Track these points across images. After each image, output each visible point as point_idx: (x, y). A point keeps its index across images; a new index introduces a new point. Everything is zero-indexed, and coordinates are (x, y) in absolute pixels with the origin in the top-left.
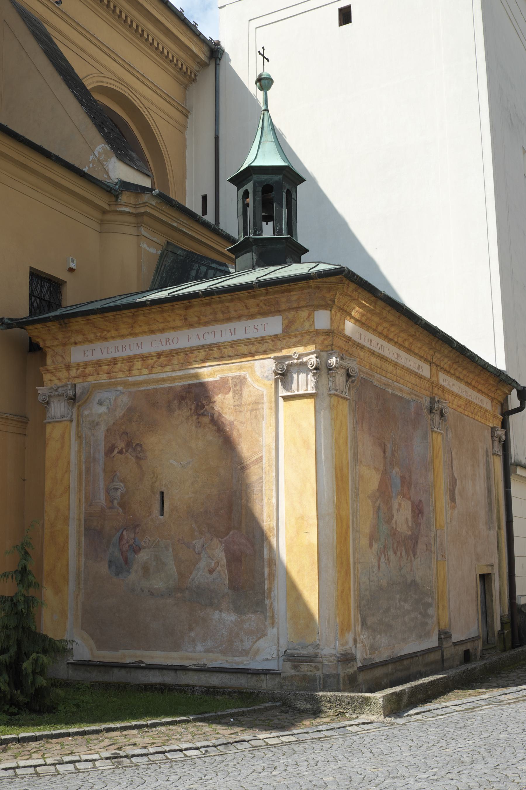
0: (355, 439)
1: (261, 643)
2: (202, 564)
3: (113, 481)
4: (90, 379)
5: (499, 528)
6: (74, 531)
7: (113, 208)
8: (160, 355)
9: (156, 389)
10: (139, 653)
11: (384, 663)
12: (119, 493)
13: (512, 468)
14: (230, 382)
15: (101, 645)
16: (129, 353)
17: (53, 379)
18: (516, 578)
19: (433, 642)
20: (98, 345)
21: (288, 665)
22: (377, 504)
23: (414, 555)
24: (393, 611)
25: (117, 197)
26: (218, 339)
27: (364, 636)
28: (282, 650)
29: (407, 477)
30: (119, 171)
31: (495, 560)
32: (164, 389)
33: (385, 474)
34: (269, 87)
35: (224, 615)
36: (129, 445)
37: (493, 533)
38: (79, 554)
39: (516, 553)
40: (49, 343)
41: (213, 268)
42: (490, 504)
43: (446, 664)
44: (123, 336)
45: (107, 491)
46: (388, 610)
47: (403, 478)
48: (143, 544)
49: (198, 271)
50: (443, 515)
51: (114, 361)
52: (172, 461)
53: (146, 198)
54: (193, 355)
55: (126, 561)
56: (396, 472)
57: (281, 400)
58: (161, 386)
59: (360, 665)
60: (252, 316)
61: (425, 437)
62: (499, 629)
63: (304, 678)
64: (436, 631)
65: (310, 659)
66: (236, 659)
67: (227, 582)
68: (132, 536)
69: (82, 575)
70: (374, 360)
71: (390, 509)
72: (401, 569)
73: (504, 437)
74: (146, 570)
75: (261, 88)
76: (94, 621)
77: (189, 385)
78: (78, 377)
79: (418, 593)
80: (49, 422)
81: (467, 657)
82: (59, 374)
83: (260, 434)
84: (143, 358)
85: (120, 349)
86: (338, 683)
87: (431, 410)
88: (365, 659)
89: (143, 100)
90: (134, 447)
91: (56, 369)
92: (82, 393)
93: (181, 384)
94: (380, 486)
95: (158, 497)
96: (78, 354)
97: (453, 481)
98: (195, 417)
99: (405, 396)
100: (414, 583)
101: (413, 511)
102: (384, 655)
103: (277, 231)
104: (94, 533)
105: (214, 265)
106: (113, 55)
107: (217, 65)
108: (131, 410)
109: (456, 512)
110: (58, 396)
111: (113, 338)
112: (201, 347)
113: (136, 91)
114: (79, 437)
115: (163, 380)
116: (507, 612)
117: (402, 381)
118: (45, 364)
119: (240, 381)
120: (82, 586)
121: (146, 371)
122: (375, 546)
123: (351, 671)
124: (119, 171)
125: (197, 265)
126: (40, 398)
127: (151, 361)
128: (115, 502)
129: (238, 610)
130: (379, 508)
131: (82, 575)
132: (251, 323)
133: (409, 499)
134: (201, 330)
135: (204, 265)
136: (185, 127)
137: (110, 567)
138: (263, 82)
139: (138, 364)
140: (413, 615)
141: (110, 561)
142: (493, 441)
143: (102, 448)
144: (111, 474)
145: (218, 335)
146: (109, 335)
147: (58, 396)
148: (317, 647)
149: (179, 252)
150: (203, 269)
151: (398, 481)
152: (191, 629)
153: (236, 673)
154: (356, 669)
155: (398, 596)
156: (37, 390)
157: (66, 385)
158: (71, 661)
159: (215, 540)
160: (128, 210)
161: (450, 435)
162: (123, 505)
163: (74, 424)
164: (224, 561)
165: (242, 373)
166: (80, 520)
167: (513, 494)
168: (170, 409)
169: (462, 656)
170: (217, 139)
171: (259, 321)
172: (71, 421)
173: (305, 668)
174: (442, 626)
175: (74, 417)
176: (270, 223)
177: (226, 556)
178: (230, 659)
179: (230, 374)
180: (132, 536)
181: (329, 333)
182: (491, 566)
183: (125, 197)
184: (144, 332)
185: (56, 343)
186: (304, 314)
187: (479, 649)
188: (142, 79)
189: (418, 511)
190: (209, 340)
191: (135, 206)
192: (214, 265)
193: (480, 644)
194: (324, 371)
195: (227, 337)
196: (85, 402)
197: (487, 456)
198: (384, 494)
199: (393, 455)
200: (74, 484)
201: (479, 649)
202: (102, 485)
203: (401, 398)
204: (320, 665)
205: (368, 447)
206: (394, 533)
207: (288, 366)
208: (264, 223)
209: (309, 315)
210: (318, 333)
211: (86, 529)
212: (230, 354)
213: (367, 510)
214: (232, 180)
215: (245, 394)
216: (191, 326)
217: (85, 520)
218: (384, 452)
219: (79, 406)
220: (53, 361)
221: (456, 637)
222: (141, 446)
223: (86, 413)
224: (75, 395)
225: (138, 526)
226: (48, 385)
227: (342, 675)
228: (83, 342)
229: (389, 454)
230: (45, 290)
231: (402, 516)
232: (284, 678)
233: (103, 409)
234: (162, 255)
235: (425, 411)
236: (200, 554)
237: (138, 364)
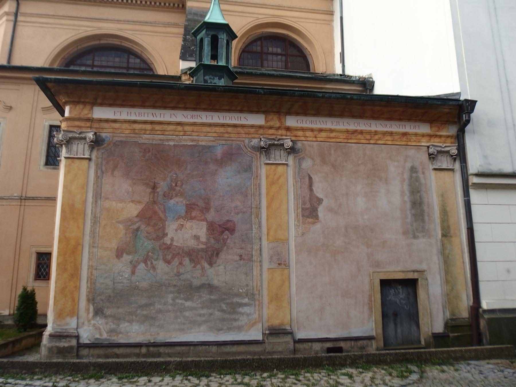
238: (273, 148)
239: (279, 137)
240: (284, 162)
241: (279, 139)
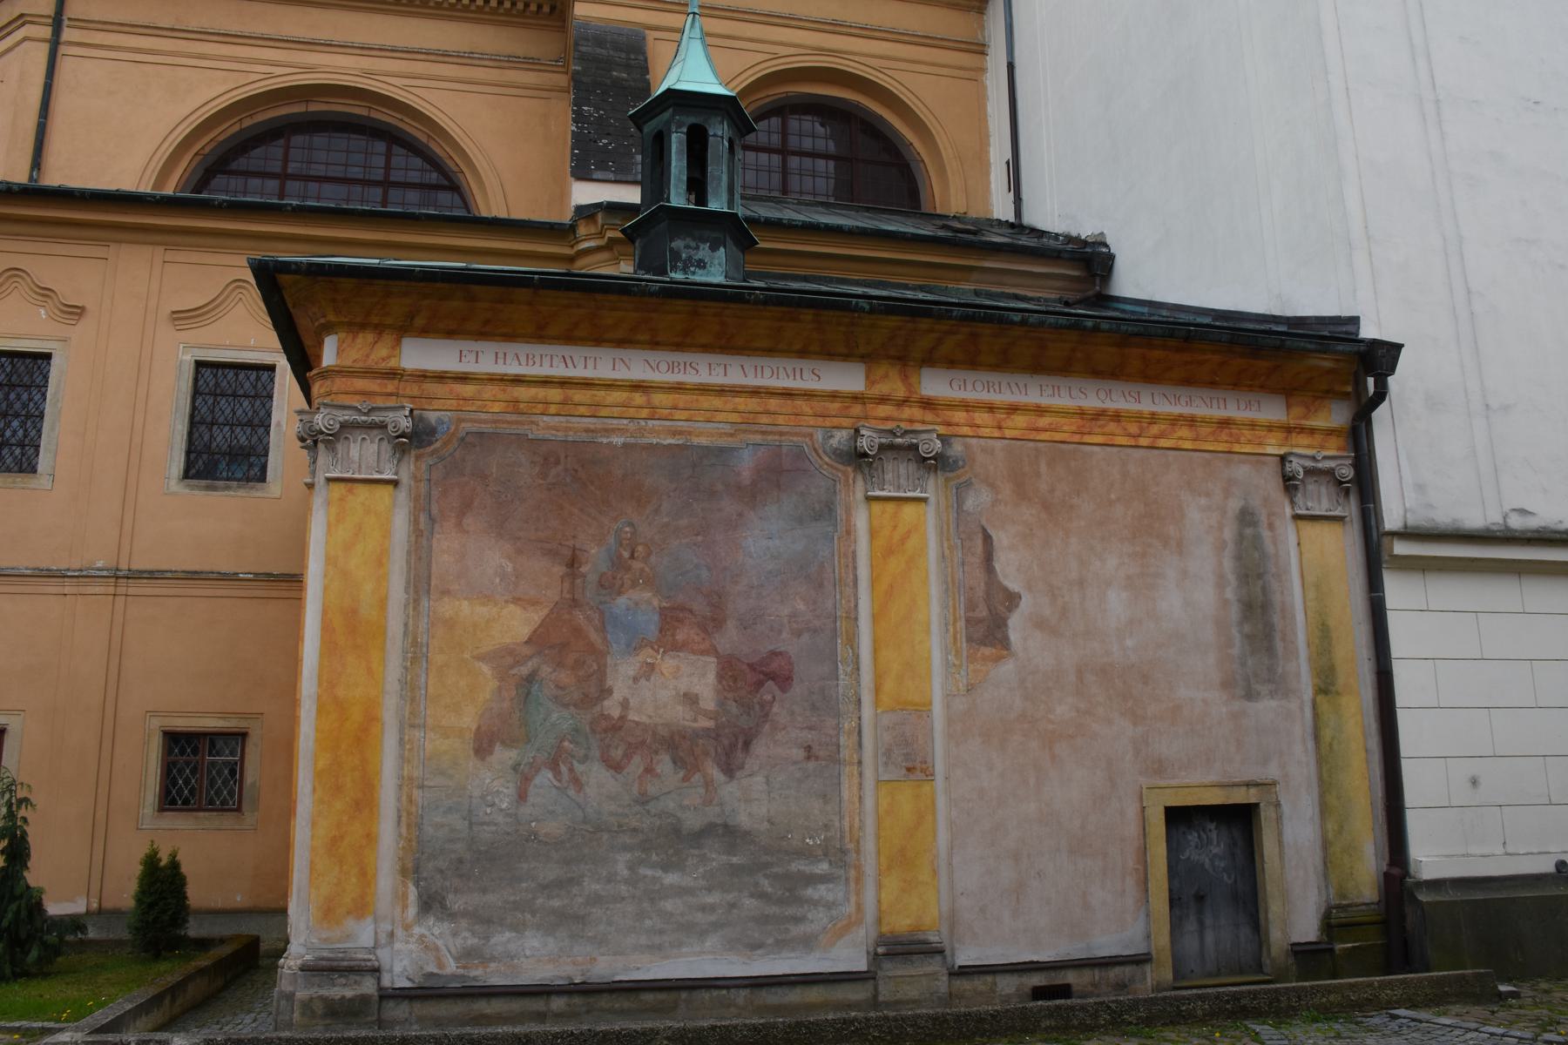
5: (1326, 686)
70: (741, 402)
89: (862, 59)
160: (592, 244)
183: (582, 230)
191: (601, 234)
238: (890, 454)
239: (904, 426)
240: (917, 494)
241: (906, 432)
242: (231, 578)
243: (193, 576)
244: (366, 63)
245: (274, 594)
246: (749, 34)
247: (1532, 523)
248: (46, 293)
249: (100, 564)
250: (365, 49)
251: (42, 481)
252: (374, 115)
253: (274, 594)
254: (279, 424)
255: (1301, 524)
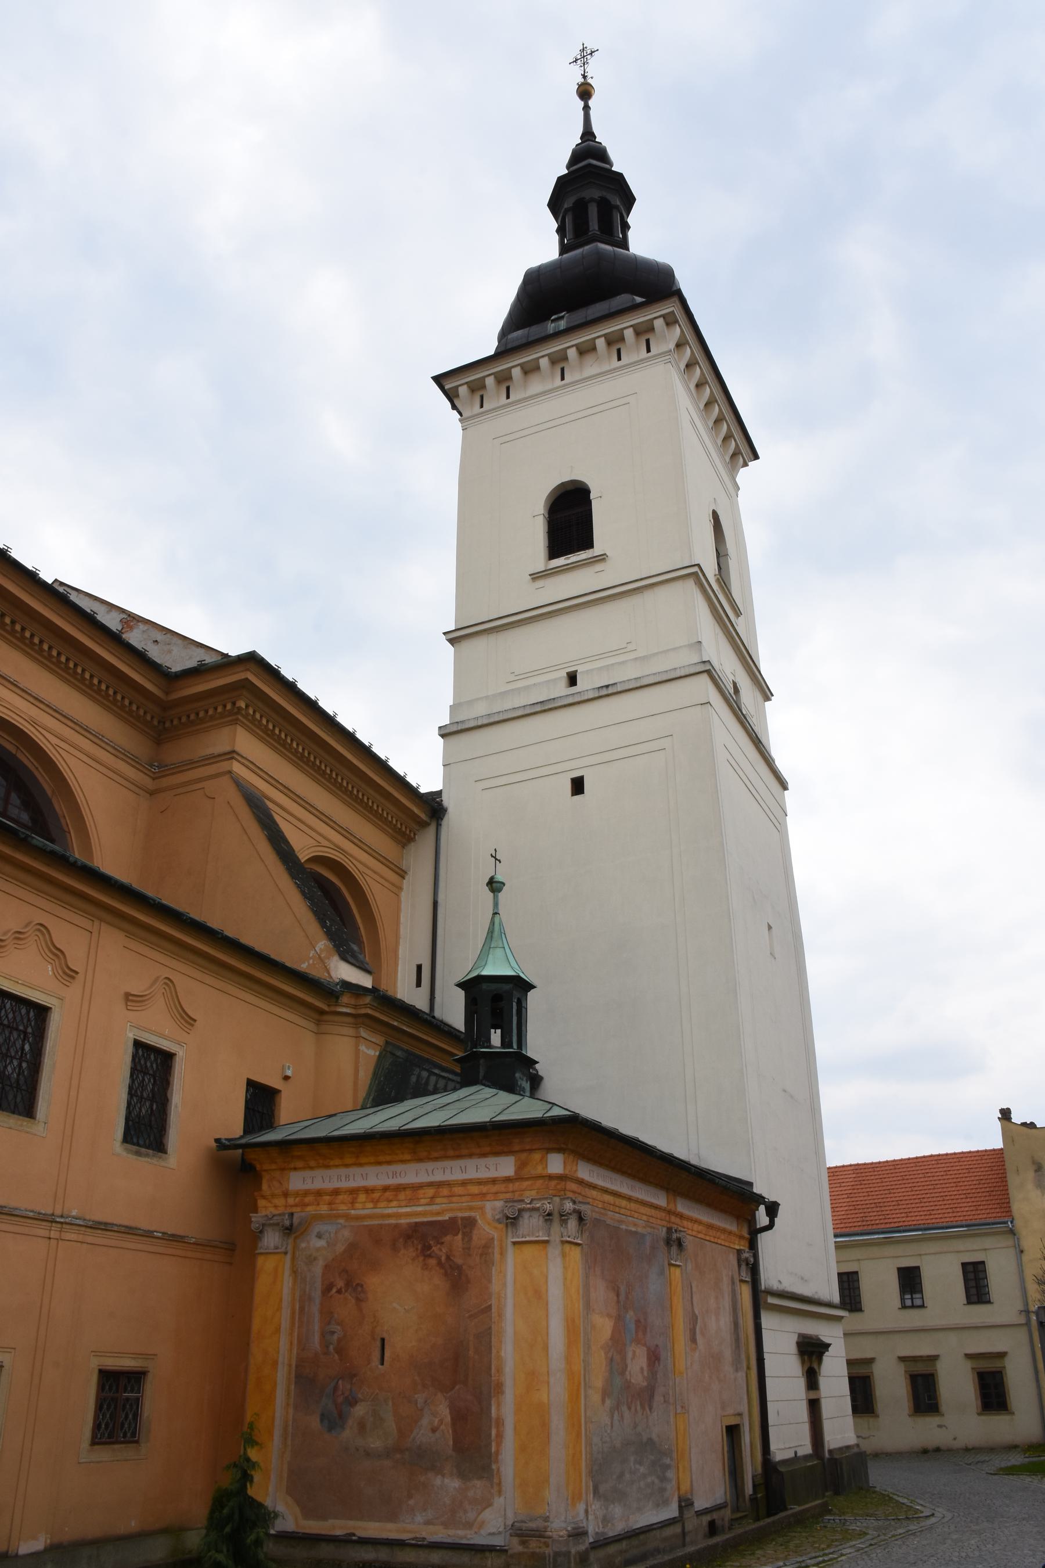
0: (587, 1287)
1: (487, 1514)
2: (425, 1422)
3: (329, 1323)
4: (309, 1208)
5: (748, 1368)
6: (282, 1376)
7: (333, 1009)
8: (386, 1189)
9: (381, 1225)
10: (351, 1523)
11: (618, 1539)
12: (335, 1337)
13: (762, 1295)
14: (460, 1222)
15: (308, 1513)
16: (352, 1184)
17: (267, 1208)
18: (770, 1429)
19: (671, 1511)
20: (319, 1173)
21: (515, 1540)
22: (610, 1355)
23: (650, 1409)
24: (627, 1476)
25: (337, 998)
26: (448, 1177)
27: (596, 1506)
28: (510, 1523)
29: (642, 1320)
30: (345, 972)
31: (744, 1408)
32: (389, 1225)
33: (619, 1319)
34: (500, 890)
35: (446, 1481)
36: (348, 1284)
37: (741, 1375)
38: (288, 1405)
39: (769, 1397)
40: (266, 1167)
41: (436, 1074)
42: (737, 1340)
43: (688, 1539)
44: (347, 1166)
45: (323, 1335)
46: (621, 1475)
47: (638, 1322)
48: (360, 1396)
49: (419, 1076)
50: (684, 1359)
51: (336, 1192)
52: (395, 1305)
53: (368, 999)
54: (421, 1192)
55: (341, 1415)
56: (630, 1316)
57: (510, 1245)
58: (387, 1222)
59: (591, 1540)
60: (484, 1155)
61: (662, 1273)
62: (751, 1492)
63: (533, 1554)
64: (676, 1499)
65: (539, 1534)
66: (460, 1533)
67: (451, 1443)
68: (348, 1387)
69: (290, 1429)
70: (608, 1198)
71: (624, 1358)
72: (635, 1426)
73: (752, 1260)
74: (362, 1426)
75: (493, 890)
76: (299, 1486)
77: (416, 1223)
78: (296, 1206)
79: (656, 1455)
80: (261, 1254)
81: (713, 1529)
82: (276, 1201)
83: (490, 1281)
84: (368, 1190)
85: (343, 1178)
86: (569, 1562)
87: (668, 1242)
88: (597, 1533)
90: (354, 1287)
91: (273, 1196)
92: (300, 1224)
93: (408, 1221)
94: (613, 1332)
95: (379, 1343)
96: (299, 1181)
97: (694, 1319)
98: (421, 1258)
99: (640, 1230)
100: (650, 1441)
101: (649, 1359)
102: (619, 1527)
103: (505, 1042)
104: (306, 1380)
105: (436, 1071)
106: (331, 823)
107: (439, 826)
108: (352, 1247)
109: (697, 1354)
110: (271, 1225)
111: (337, 1166)
112: (431, 1184)
113: (351, 856)
114: (294, 1272)
115: (389, 1216)
116: (759, 1470)
117: (636, 1215)
118: (260, 1189)
119: (470, 1223)
120: (289, 1442)
121: (371, 1205)
122: (608, 1402)
123: (582, 1548)
124: (345, 972)
125: (418, 1070)
126: (254, 1226)
127: (376, 1195)
128: (331, 1347)
129: (462, 1475)
130: (612, 1360)
131: (290, 1429)
132: (482, 1162)
133: (645, 1345)
134: (430, 1165)
135: (425, 1069)
136: (401, 889)
137: (322, 1421)
138: (494, 885)
139: (362, 1197)
140: (649, 1480)
141: (322, 1415)
142: (739, 1266)
143: (319, 1285)
144: (327, 1315)
145: (448, 1171)
146: (332, 1163)
147: (271, 1225)
148: (546, 1519)
149: (399, 1053)
150: (425, 1074)
151: (633, 1326)
152: (410, 1497)
153: (459, 1549)
154: (587, 1545)
155: (632, 1458)
156: (250, 1218)
157: (283, 1214)
158: (272, 1532)
159: (439, 1395)
161: (690, 1267)
162: (339, 1351)
163: (289, 1257)
164: (448, 1419)
165: (473, 1214)
166: (290, 1365)
167: (763, 1326)
168: (395, 1249)
169: (707, 1529)
170: (435, 904)
171: (491, 1161)
172: (286, 1253)
173: (534, 1545)
174: (682, 1492)
175: (290, 1248)
176: (499, 1031)
177: (451, 1413)
178: (451, 1532)
179: (460, 1215)
180: (348, 1387)
181: (561, 1178)
182: (740, 1415)
183: (345, 999)
184: (370, 1164)
185: (274, 1167)
186: (537, 1156)
187: (726, 1519)
188: (359, 843)
189: (654, 1357)
190: (438, 1177)
191: (355, 1007)
192: (436, 1071)
193: (727, 1513)
194: (556, 1217)
195: (457, 1176)
196: (302, 1234)
197: (733, 1283)
198: (617, 1344)
199: (627, 1298)
200: (285, 1324)
201: (726, 1519)
202: (317, 1327)
203: (636, 1233)
204: (550, 1541)
205: (600, 1292)
206: (628, 1386)
207: (520, 1211)
208: (493, 1031)
209: (542, 1158)
210: (551, 1177)
211: (296, 1377)
212: (461, 1193)
213: (599, 1361)
214: (461, 985)
215: (475, 1237)
216: (420, 1160)
217: (297, 1367)
218: (618, 1295)
219: (296, 1238)
220: (269, 1186)
221: (700, 1504)
222: (362, 1286)
223: (303, 1245)
224: (292, 1225)
225: (355, 1375)
226: (263, 1212)
227: (573, 1551)
228: (303, 1168)
229: (622, 1297)
230: (261, 1101)
231: (637, 1364)
232: (512, 1556)
233: (322, 1243)
234: (379, 1056)
235: (662, 1243)
236: (422, 1410)
237: (362, 1197)
242: (148, 1234)
243: (130, 1231)
244: (34, 712)
245: (140, 1246)
246: (322, 831)
247: (781, 1287)
248: (58, 953)
249: (74, 1213)
250: (37, 701)
251: (37, 1128)
252: (20, 756)
253: (140, 1246)
254: (176, 1107)
255: (567, 1247)
